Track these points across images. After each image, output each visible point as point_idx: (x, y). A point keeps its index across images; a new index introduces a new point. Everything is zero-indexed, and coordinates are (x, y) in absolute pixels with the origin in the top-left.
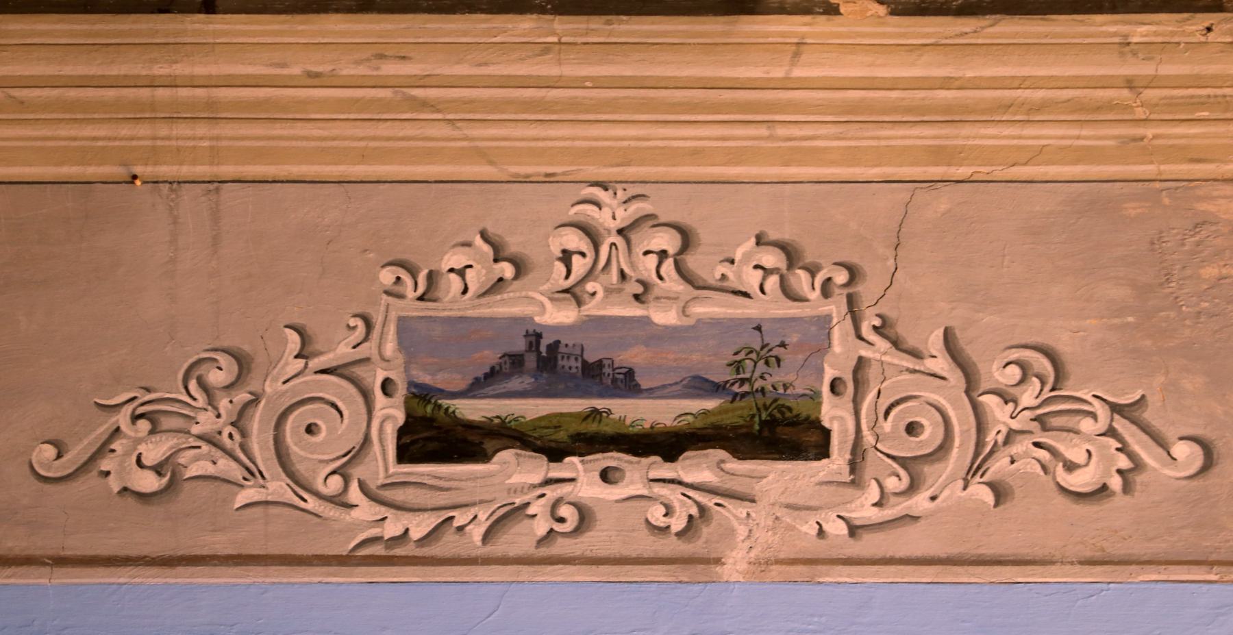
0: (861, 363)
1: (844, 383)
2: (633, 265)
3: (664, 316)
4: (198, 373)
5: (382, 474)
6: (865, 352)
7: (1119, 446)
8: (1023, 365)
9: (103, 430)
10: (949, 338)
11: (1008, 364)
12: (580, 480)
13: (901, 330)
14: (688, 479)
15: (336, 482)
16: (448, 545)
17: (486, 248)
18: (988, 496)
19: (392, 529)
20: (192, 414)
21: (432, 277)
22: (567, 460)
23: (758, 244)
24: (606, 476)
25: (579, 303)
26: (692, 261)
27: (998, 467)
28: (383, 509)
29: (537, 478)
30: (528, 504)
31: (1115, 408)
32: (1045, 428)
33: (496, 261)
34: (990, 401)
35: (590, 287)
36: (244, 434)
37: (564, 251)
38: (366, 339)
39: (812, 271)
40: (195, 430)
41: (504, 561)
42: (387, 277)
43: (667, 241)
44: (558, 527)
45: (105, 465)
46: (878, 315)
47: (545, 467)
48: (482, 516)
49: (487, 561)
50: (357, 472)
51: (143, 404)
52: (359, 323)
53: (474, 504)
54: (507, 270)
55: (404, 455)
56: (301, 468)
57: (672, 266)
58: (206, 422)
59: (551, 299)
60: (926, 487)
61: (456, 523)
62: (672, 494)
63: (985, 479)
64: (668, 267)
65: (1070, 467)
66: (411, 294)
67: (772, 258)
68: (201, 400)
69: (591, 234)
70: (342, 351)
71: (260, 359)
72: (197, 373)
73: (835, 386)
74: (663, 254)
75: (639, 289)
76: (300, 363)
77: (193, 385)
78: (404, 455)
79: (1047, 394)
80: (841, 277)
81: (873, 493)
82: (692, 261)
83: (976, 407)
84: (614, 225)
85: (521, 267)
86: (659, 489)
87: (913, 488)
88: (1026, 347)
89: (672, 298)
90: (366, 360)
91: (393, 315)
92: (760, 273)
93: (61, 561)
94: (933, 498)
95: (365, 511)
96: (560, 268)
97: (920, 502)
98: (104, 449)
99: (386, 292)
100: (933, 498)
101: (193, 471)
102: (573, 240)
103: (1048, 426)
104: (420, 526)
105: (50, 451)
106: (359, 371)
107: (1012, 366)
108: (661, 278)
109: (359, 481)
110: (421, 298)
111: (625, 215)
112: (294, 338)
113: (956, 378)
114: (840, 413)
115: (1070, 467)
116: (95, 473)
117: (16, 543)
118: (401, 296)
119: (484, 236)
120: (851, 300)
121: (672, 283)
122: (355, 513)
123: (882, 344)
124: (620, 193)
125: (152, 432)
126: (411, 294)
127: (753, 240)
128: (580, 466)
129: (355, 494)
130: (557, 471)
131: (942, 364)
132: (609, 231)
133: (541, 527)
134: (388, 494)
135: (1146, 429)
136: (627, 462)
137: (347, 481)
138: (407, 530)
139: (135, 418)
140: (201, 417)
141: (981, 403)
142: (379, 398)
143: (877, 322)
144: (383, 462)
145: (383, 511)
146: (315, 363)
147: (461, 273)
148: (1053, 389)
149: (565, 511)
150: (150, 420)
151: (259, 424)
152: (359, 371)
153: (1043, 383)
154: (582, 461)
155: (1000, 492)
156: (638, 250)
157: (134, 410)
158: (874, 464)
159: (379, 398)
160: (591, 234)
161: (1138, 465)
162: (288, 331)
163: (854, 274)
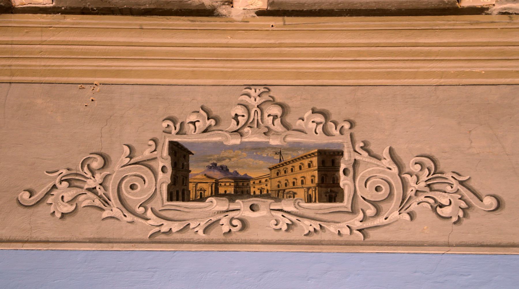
0: (356, 163)
1: (349, 170)
2: (262, 119)
3: (274, 142)
4: (88, 163)
5: (160, 205)
6: (358, 157)
7: (460, 197)
8: (421, 164)
9: (50, 185)
10: (391, 151)
11: (416, 163)
12: (242, 209)
13: (372, 148)
14: (285, 209)
15: (142, 209)
16: (187, 235)
17: (205, 114)
18: (408, 217)
19: (164, 229)
20: (85, 180)
21: (182, 124)
22: (237, 201)
23: (313, 113)
24: (252, 208)
25: (242, 136)
26: (288, 119)
27: (413, 206)
28: (162, 220)
29: (225, 208)
30: (220, 220)
31: (461, 183)
32: (431, 190)
33: (208, 119)
34: (408, 176)
35: (246, 129)
36: (105, 189)
37: (236, 115)
38: (155, 150)
39: (336, 124)
40: (86, 187)
41: (189, 242)
42: (165, 124)
43: (277, 111)
44: (234, 229)
45: (50, 200)
46: (363, 142)
47: (228, 204)
48: (202, 224)
49: (182, 242)
50: (149, 206)
51: (64, 176)
52: (151, 143)
53: (188, 220)
54: (212, 122)
55: (170, 198)
56: (130, 203)
57: (280, 121)
58: (91, 183)
59: (230, 135)
60: (383, 213)
61: (192, 226)
62: (279, 214)
63: (408, 210)
64: (278, 121)
65: (441, 206)
66: (174, 132)
67: (320, 118)
68: (89, 175)
69: (247, 107)
70: (147, 154)
71: (113, 158)
72: (88, 163)
73: (345, 172)
74: (275, 117)
75: (266, 130)
76: (128, 159)
77: (86, 168)
78: (170, 198)
79: (430, 177)
80: (347, 126)
81: (361, 216)
82: (288, 119)
83: (402, 179)
84: (256, 104)
85: (217, 121)
86: (274, 213)
87: (377, 214)
88: (422, 156)
89: (277, 134)
90: (155, 159)
91: (167, 141)
92: (315, 124)
93: (47, 242)
94: (386, 219)
95: (154, 221)
96: (234, 122)
97: (380, 220)
98: (48, 194)
99: (164, 132)
100: (386, 219)
101: (84, 204)
102: (240, 110)
103: (433, 189)
104: (176, 227)
105: (26, 195)
106: (152, 163)
107: (418, 165)
108: (274, 125)
109: (152, 209)
110: (177, 134)
111: (259, 101)
112: (127, 150)
113: (395, 170)
114: (348, 182)
115: (441, 206)
116: (45, 204)
117: (5, 233)
118: (170, 133)
119: (202, 108)
120: (351, 136)
121: (278, 127)
122: (150, 222)
123: (365, 154)
124: (257, 91)
125: (70, 186)
126: (174, 132)
127: (311, 111)
128: (241, 203)
129: (149, 214)
130: (233, 206)
131: (387, 162)
132: (254, 106)
133: (226, 229)
134: (164, 214)
135: (469, 189)
136: (261, 201)
137: (146, 209)
138: (171, 229)
139: (61, 181)
140: (88, 181)
141: (404, 178)
142: (160, 175)
143: (362, 145)
144: (161, 200)
145: (160, 221)
146: (133, 161)
147: (194, 123)
148: (434, 174)
149: (235, 222)
150: (68, 182)
151: (112, 185)
152: (152, 163)
153: (429, 170)
154: (243, 202)
155: (412, 215)
156: (266, 115)
157: (62, 178)
158: (361, 204)
159: (160, 175)
160: (247, 107)
161: (470, 206)
162: (124, 146)
163: (352, 124)
